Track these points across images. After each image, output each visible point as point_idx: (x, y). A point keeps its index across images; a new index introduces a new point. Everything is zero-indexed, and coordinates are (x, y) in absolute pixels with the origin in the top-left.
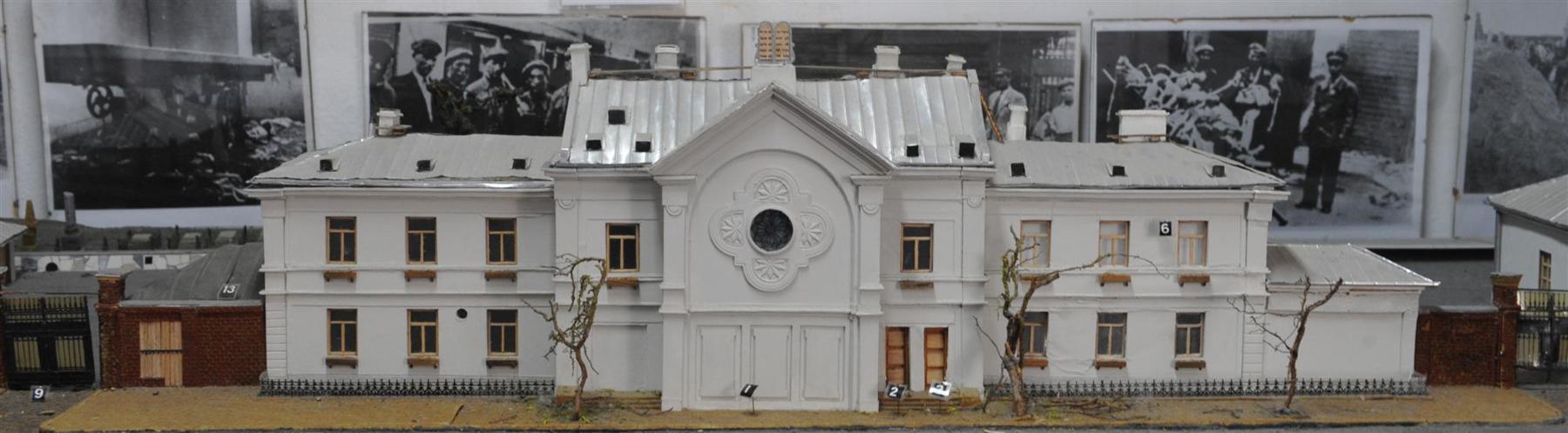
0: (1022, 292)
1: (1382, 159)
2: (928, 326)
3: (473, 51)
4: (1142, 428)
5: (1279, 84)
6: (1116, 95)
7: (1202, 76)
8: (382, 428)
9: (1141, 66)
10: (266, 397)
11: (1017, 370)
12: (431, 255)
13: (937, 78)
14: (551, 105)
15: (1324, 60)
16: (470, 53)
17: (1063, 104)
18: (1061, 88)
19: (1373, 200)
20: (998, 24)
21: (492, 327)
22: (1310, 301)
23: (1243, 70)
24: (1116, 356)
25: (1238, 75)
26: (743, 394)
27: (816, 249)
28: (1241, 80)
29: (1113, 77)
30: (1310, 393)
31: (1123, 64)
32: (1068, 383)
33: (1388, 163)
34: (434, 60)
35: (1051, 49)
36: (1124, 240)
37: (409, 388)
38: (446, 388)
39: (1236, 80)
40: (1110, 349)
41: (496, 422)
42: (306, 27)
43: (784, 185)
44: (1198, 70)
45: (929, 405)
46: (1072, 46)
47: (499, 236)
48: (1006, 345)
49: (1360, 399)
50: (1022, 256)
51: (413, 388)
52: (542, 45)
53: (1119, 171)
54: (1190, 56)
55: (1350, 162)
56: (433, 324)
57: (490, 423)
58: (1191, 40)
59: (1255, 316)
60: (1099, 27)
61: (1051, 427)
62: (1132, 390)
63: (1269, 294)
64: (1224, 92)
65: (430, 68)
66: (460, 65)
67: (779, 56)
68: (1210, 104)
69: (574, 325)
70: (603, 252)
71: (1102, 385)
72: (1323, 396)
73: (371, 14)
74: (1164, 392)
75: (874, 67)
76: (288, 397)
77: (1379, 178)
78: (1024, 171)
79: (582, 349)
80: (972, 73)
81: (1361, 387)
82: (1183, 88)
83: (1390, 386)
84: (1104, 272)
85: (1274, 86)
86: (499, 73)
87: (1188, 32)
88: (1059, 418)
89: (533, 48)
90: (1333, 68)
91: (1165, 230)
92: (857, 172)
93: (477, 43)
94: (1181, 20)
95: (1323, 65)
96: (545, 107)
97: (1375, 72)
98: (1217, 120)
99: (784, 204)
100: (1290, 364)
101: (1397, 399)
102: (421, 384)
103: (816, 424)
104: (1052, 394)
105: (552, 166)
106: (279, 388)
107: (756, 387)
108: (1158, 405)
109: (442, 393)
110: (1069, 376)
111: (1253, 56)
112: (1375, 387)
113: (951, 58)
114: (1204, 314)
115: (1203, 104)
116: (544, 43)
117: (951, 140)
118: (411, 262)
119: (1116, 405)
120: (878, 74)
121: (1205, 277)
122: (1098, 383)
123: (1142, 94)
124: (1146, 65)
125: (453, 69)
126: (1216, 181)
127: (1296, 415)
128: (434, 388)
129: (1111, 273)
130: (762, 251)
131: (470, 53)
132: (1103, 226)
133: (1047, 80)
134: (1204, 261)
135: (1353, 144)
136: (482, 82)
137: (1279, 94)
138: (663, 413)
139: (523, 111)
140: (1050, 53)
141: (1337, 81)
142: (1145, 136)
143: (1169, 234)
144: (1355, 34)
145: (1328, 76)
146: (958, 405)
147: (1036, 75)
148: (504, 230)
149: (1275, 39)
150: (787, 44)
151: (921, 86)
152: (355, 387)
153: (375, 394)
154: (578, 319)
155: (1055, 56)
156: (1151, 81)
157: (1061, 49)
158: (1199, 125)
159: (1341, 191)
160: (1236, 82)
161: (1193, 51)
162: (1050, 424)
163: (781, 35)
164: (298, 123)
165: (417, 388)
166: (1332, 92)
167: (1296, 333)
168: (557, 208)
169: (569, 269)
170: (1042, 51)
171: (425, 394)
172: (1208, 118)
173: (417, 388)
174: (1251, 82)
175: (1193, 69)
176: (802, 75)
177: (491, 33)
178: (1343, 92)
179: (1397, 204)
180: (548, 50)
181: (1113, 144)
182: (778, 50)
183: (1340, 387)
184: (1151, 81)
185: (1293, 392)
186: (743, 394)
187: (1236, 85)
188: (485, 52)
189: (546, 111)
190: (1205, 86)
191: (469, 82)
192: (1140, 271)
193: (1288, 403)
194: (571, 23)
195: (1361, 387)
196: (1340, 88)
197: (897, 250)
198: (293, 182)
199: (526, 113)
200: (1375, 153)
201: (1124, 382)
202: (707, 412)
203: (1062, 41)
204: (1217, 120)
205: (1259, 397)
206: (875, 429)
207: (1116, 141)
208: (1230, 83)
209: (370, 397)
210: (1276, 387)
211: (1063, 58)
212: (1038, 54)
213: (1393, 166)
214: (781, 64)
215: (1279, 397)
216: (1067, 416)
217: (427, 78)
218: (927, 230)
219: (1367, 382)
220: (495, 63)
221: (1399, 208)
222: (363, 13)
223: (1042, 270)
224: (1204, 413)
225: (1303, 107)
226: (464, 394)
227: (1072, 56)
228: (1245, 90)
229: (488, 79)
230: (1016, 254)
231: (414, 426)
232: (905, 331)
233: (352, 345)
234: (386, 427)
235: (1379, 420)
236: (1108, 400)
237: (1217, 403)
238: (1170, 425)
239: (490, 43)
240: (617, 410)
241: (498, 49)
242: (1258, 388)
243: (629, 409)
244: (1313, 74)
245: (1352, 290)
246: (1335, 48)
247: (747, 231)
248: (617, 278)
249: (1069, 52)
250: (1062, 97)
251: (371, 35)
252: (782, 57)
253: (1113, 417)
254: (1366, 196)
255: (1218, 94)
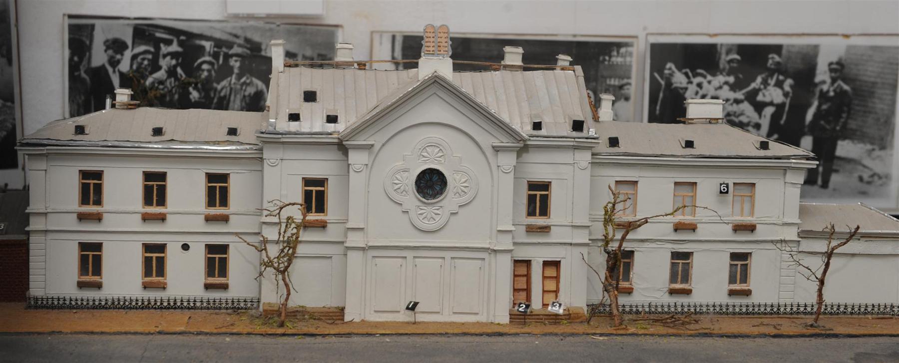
0: (619, 236)
1: (869, 147)
2: (546, 260)
3: (155, 48)
4: (709, 337)
5: (791, 86)
6: (664, 93)
7: (731, 79)
8: (132, 331)
9: (684, 71)
10: (32, 310)
11: (614, 293)
12: (162, 202)
13: (551, 71)
14: (217, 93)
15: (826, 68)
16: (152, 49)
17: (623, 100)
18: (621, 87)
19: (861, 179)
20: (575, 36)
21: (209, 258)
22: (834, 243)
23: (763, 76)
24: (684, 285)
25: (759, 79)
26: (408, 308)
27: (464, 199)
28: (762, 83)
29: (662, 78)
30: (831, 314)
31: (670, 69)
32: (649, 304)
33: (873, 150)
34: (122, 55)
35: (614, 56)
36: (692, 196)
37: (146, 303)
38: (175, 304)
39: (757, 83)
40: (679, 279)
41: (220, 328)
42: (17, 26)
43: (441, 149)
44: (729, 74)
45: (547, 319)
46: (631, 54)
47: (216, 187)
48: (606, 274)
49: (868, 318)
50: (619, 207)
51: (149, 303)
52: (211, 45)
53: (689, 144)
54: (723, 64)
55: (844, 148)
56: (162, 255)
57: (216, 328)
58: (724, 51)
59: (792, 253)
60: (654, 40)
61: (641, 335)
62: (698, 310)
63: (800, 239)
64: (748, 93)
65: (119, 62)
66: (144, 59)
67: (440, 51)
68: (737, 102)
69: (280, 254)
70: (299, 198)
71: (675, 306)
72: (840, 316)
73: (71, 17)
74: (722, 312)
75: (503, 63)
76: (51, 310)
77: (867, 162)
78: (618, 143)
79: (286, 273)
80: (578, 68)
81: (869, 309)
82: (716, 89)
83: (891, 309)
84: (677, 221)
85: (787, 88)
86: (175, 67)
87: (722, 45)
88: (645, 328)
89: (203, 47)
90: (833, 75)
91: (724, 189)
92: (497, 141)
93: (157, 43)
94: (716, 35)
95: (825, 72)
96: (212, 95)
97: (865, 78)
98: (742, 114)
99: (440, 163)
100: (818, 289)
101: (896, 319)
102: (155, 301)
103: (464, 331)
104: (638, 312)
105: (262, 133)
106: (42, 303)
107: (418, 303)
108: (718, 320)
109: (172, 308)
110: (649, 300)
111: (771, 65)
112: (879, 309)
113: (561, 57)
114: (751, 253)
115: (731, 101)
116: (213, 43)
117: (565, 119)
118: (146, 207)
119: (686, 320)
120: (506, 67)
121: (753, 225)
122: (672, 304)
123: (685, 93)
124: (688, 70)
125: (138, 62)
126: (763, 153)
127: (823, 328)
128: (165, 304)
129: (683, 221)
130: (423, 200)
131: (152, 49)
132: (679, 187)
133: (610, 81)
134: (752, 213)
135: (848, 134)
136: (161, 74)
137: (791, 95)
138: (346, 322)
139: (194, 98)
140: (614, 59)
141: (836, 85)
142: (706, 119)
143: (727, 192)
144: (849, 48)
145: (829, 81)
146: (569, 319)
147: (603, 77)
148: (220, 183)
149: (789, 52)
150: (446, 42)
151: (538, 77)
152: (103, 303)
153: (119, 308)
154: (282, 251)
155: (617, 62)
156: (691, 83)
157: (622, 56)
158: (728, 118)
159: (837, 171)
160: (757, 84)
161: (725, 60)
162: (640, 332)
163: (442, 35)
164: (9, 104)
165: (153, 303)
166: (832, 94)
167: (823, 267)
168: (265, 165)
169: (278, 211)
170: (607, 58)
171: (158, 309)
172: (735, 113)
173: (153, 303)
174: (769, 85)
175: (724, 74)
176: (457, 68)
177: (169, 34)
178: (841, 93)
179: (880, 182)
180: (216, 49)
181: (681, 125)
182: (439, 46)
183: (853, 309)
184: (691, 83)
185: (818, 313)
186: (408, 308)
187: (757, 87)
188: (164, 49)
189: (213, 98)
190: (734, 87)
191: (151, 73)
192: (704, 221)
193: (816, 320)
194: (234, 28)
195: (869, 309)
196: (838, 90)
197: (525, 201)
198: (54, 142)
199: (197, 99)
200: (864, 142)
201: (692, 304)
202: (380, 322)
203: (623, 50)
204: (742, 114)
205: (793, 316)
206: (509, 335)
207: (684, 123)
208: (753, 85)
209: (115, 310)
210: (805, 309)
211: (623, 63)
212: (605, 60)
213: (877, 153)
214: (441, 58)
215: (807, 316)
216: (652, 328)
217: (116, 70)
218: (546, 186)
219: (873, 306)
220: (172, 59)
221: (881, 185)
222: (64, 15)
223: (631, 219)
224: (753, 326)
225: (809, 105)
226: (189, 308)
227: (631, 62)
228: (764, 91)
229: (167, 72)
230: (614, 205)
231: (157, 330)
232: (528, 263)
233: (98, 271)
234: (136, 331)
235: (885, 332)
236: (682, 317)
237: (762, 320)
238: (730, 335)
239: (169, 43)
240: (311, 320)
241: (175, 47)
242: (792, 309)
243: (319, 319)
244: (818, 79)
245: (861, 237)
246: (835, 59)
247: (412, 185)
248: (310, 220)
249: (628, 59)
250: (622, 95)
251: (70, 33)
252: (442, 52)
253: (687, 329)
254: (856, 175)
255: (744, 94)
